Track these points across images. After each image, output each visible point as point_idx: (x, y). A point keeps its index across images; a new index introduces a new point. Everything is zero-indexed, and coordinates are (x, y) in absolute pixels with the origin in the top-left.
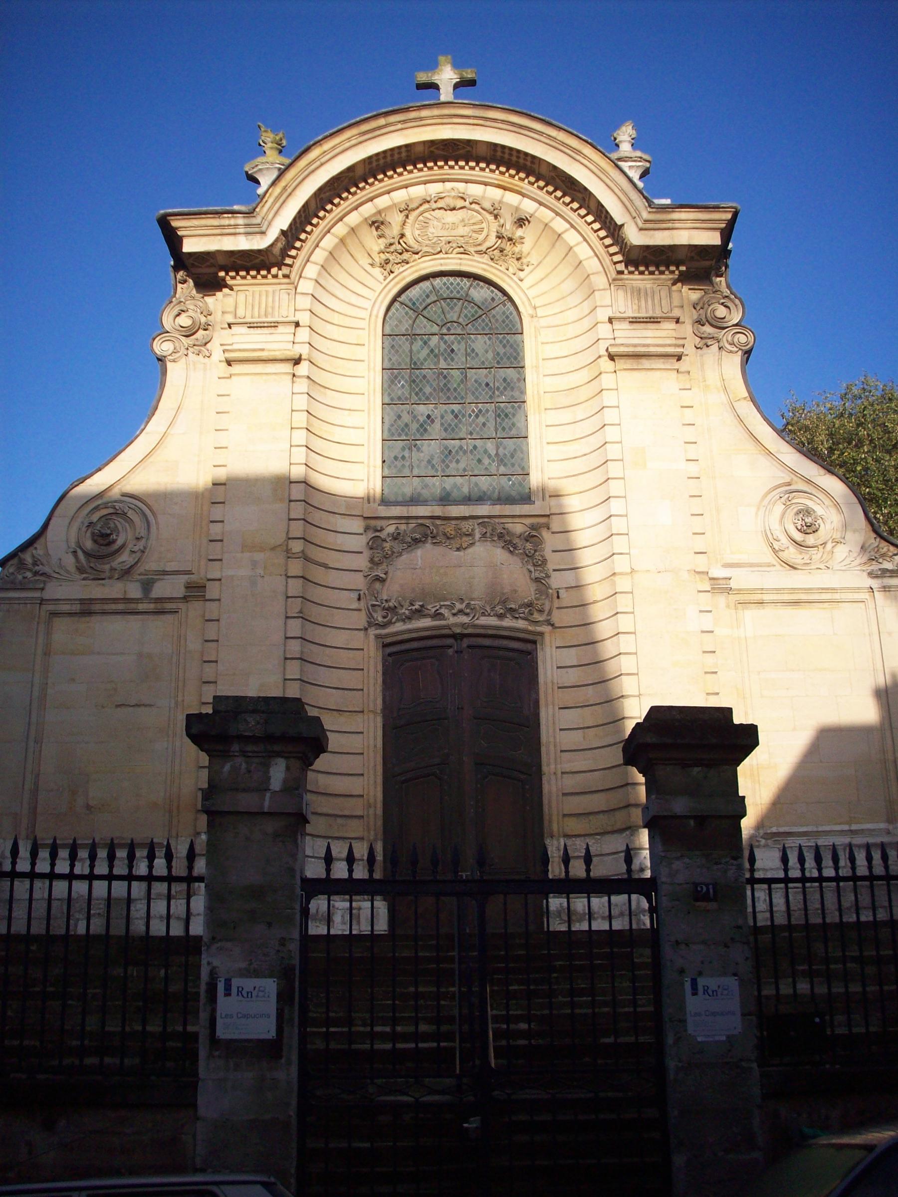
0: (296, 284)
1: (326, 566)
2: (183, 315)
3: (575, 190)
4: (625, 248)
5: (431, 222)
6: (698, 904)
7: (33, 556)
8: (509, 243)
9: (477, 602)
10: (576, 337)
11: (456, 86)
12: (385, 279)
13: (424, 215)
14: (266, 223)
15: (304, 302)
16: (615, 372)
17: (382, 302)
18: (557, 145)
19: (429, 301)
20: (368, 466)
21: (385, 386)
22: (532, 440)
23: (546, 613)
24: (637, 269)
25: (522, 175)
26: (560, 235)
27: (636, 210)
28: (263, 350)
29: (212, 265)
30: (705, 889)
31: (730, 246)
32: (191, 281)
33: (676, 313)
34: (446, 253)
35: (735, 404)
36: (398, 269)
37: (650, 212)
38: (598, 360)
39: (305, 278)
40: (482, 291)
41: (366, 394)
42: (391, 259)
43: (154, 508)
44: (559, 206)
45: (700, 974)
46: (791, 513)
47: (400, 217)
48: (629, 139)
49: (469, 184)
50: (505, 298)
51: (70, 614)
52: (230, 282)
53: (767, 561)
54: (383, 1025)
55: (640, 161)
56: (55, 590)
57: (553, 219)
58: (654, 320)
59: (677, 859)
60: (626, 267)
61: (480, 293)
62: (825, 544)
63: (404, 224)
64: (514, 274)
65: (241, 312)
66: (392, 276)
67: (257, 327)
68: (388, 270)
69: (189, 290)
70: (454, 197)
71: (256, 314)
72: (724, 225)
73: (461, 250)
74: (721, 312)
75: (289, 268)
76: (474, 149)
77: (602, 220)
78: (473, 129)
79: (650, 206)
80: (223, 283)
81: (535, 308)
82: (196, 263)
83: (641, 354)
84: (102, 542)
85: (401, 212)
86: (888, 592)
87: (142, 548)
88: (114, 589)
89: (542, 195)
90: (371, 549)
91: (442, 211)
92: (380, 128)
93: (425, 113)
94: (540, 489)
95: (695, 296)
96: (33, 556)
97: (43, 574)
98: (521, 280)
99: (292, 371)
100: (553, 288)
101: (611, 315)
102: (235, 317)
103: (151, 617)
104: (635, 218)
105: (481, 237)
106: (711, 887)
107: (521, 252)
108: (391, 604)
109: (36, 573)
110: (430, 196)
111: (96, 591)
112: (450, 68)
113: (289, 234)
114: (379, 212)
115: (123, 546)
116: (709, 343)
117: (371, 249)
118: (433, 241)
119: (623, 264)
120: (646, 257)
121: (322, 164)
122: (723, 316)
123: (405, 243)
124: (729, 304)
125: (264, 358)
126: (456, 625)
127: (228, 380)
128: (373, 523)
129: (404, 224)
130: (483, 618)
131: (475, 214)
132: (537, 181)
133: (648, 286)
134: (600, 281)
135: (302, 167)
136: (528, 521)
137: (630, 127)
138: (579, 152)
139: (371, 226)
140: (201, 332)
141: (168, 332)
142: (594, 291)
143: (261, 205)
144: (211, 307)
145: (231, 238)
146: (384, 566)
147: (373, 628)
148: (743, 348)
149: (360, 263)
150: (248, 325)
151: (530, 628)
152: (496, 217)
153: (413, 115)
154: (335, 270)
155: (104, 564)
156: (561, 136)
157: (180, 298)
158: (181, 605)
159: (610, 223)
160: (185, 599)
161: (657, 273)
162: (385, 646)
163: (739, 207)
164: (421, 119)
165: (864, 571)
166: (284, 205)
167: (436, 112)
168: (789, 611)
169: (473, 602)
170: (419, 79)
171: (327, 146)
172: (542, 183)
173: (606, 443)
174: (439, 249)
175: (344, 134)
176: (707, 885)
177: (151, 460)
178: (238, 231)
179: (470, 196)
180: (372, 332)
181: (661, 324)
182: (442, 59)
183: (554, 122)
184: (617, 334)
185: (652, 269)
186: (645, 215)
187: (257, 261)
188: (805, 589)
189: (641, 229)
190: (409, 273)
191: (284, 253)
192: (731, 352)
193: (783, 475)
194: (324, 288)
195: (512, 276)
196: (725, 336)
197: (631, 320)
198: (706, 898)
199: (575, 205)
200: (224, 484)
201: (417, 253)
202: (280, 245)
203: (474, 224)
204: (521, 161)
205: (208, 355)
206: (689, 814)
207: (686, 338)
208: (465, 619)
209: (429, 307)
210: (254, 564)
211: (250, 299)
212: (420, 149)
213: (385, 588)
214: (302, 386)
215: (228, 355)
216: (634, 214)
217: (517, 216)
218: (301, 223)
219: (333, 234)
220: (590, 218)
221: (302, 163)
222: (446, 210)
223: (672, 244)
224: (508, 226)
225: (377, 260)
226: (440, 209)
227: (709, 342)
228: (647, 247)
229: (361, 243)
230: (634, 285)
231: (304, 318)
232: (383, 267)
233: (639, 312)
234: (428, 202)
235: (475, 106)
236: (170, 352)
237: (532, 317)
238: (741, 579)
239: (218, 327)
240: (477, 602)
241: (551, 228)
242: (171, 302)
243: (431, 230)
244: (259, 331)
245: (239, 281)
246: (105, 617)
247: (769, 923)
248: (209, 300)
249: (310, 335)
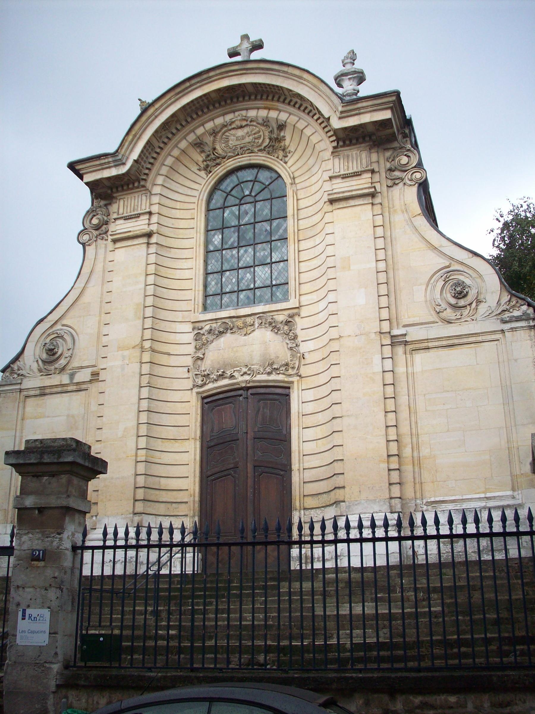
1: (169, 354)
2: (94, 218)
5: (229, 138)
6: (32, 563)
7: (18, 366)
9: (255, 366)
12: (207, 176)
13: (226, 134)
17: (205, 191)
23: (296, 369)
28: (130, 231)
30: (37, 553)
41: (195, 248)
43: (77, 331)
45: (28, 606)
46: (448, 287)
47: (212, 138)
51: (35, 396)
53: (432, 320)
54: (95, 630)
56: (27, 384)
59: (25, 534)
62: (470, 304)
66: (211, 174)
70: (240, 120)
73: (249, 151)
74: (404, 160)
84: (50, 353)
86: (515, 332)
87: (70, 355)
88: (55, 380)
90: (196, 340)
91: (235, 130)
92: (187, 88)
96: (18, 366)
97: (22, 375)
102: (118, 214)
103: (74, 393)
105: (260, 141)
106: (41, 552)
108: (206, 373)
109: (19, 375)
111: (48, 381)
115: (61, 355)
124: (410, 154)
126: (242, 382)
128: (197, 325)
130: (258, 376)
136: (287, 313)
145: (108, 170)
146: (203, 350)
147: (196, 388)
151: (286, 379)
155: (52, 366)
158: (89, 385)
160: (91, 381)
162: (203, 398)
164: (210, 77)
165: (498, 319)
168: (446, 351)
169: (253, 367)
176: (39, 551)
178: (110, 165)
179: (249, 117)
186: (340, 109)
188: (457, 336)
190: (220, 171)
192: (410, 185)
193: (443, 261)
196: (407, 176)
198: (38, 559)
201: (224, 158)
203: (255, 134)
206: (33, 507)
208: (247, 378)
210: (124, 357)
213: (204, 363)
225: (202, 166)
226: (233, 129)
227: (397, 182)
231: (155, 209)
234: (226, 126)
236: (87, 240)
238: (414, 334)
240: (255, 366)
243: (230, 142)
244: (130, 221)
246: (52, 396)
247: (425, 562)
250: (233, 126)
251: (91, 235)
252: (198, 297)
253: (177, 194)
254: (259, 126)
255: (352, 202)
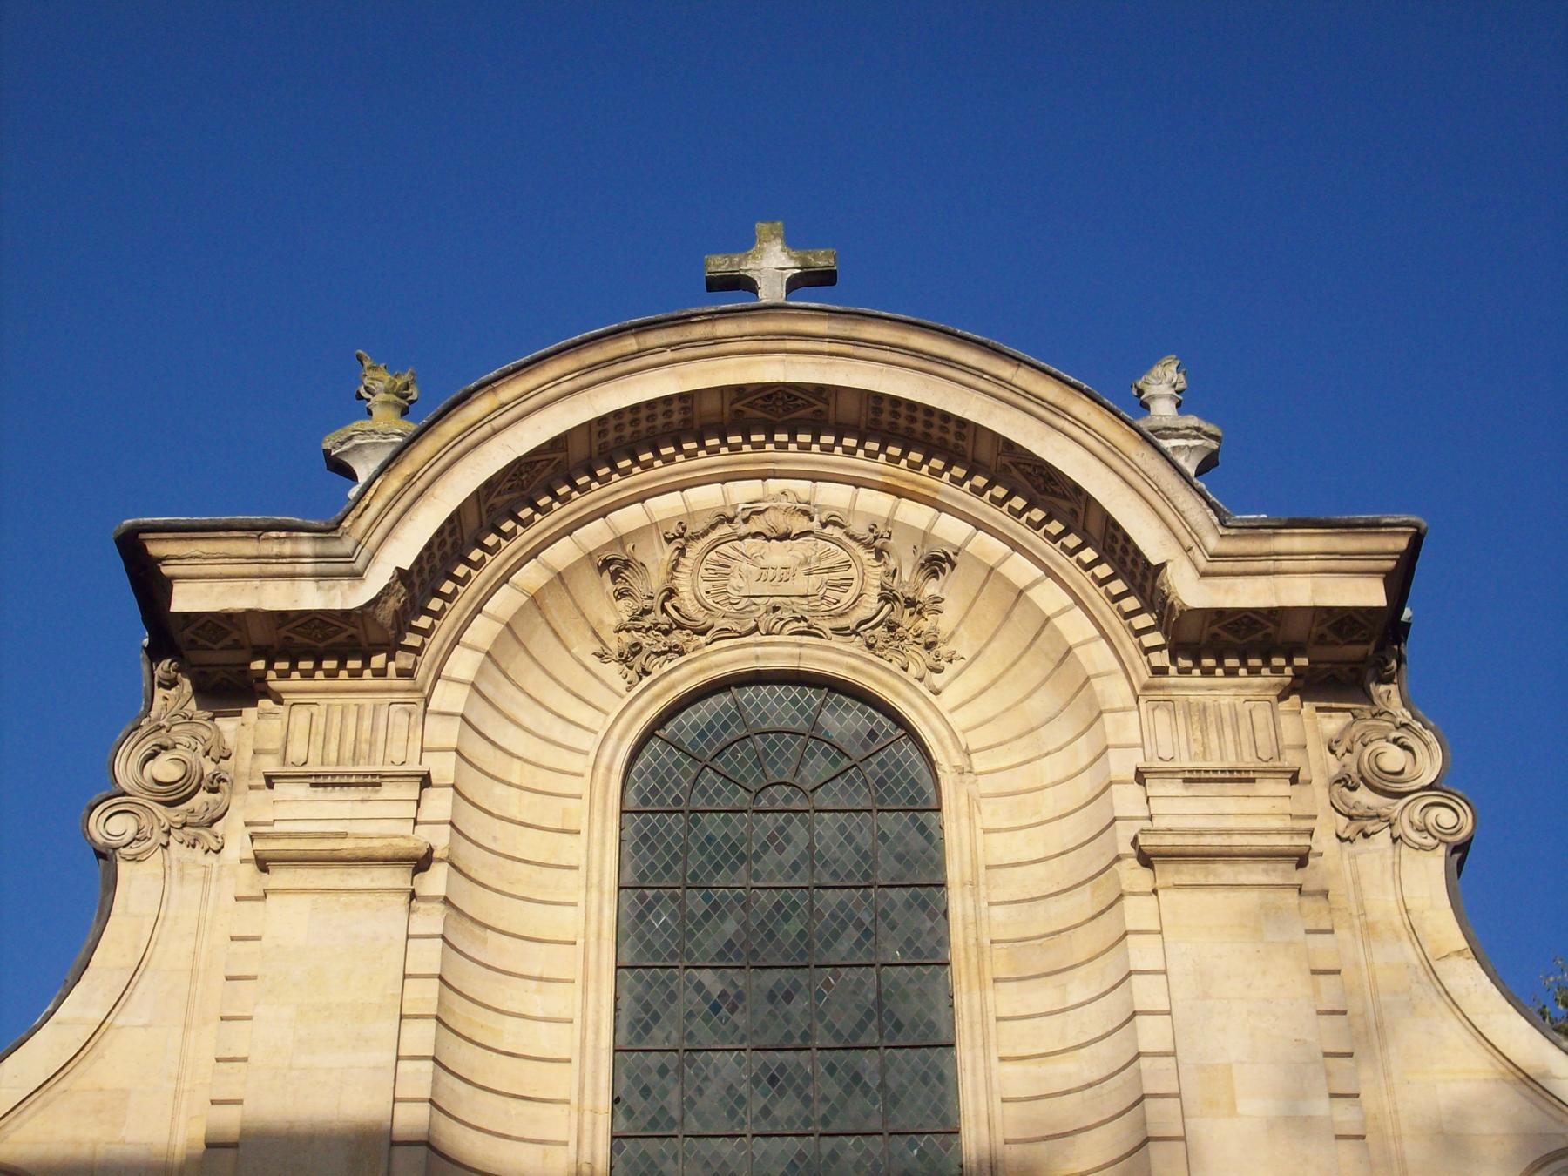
0: (427, 692)
2: (164, 757)
3: (1054, 493)
4: (1169, 617)
5: (734, 565)
8: (908, 611)
10: (1061, 817)
11: (793, 285)
13: (718, 549)
14: (365, 554)
15: (444, 733)
16: (1155, 892)
17: (621, 738)
18: (1013, 397)
19: (727, 737)
20: (580, 1110)
21: (624, 925)
22: (966, 1053)
24: (1197, 663)
25: (937, 463)
26: (1021, 592)
27: (1193, 531)
29: (237, 646)
31: (1407, 613)
32: (187, 681)
33: (1291, 759)
34: (768, 633)
35: (1438, 966)
36: (659, 667)
37: (1221, 536)
38: (1115, 866)
39: (449, 679)
40: (849, 718)
41: (580, 941)
42: (644, 642)
44: (1018, 529)
47: (669, 552)
48: (1172, 391)
49: (819, 484)
50: (901, 732)
52: (276, 684)
55: (1196, 437)
57: (1006, 557)
58: (1240, 777)
60: (1173, 660)
61: (844, 722)
63: (674, 569)
64: (921, 680)
65: (297, 751)
66: (646, 680)
67: (334, 785)
68: (637, 667)
69: (181, 703)
71: (333, 756)
72: (1390, 565)
75: (412, 656)
76: (832, 408)
77: (1116, 557)
78: (830, 364)
79: (1222, 523)
80: (259, 686)
81: (968, 753)
82: (201, 642)
83: (1214, 850)
85: (669, 541)
89: (981, 507)
91: (760, 541)
92: (624, 358)
93: (724, 328)
94: (986, 1166)
95: (1333, 724)
98: (937, 693)
99: (409, 886)
100: (1008, 709)
101: (1142, 764)
102: (284, 761)
104: (1190, 549)
105: (846, 598)
107: (935, 631)
110: (735, 506)
112: (780, 247)
113: (417, 581)
114: (620, 541)
116: (1369, 829)
117: (601, 622)
118: (737, 607)
119: (1166, 652)
120: (1215, 636)
121: (495, 432)
122: (1398, 769)
123: (677, 609)
124: (1411, 741)
125: (344, 854)
127: (260, 904)
129: (674, 569)
131: (833, 547)
132: (969, 476)
133: (1225, 701)
134: (1115, 691)
135: (451, 435)
137: (1174, 367)
138: (1061, 411)
139: (601, 569)
140: (202, 796)
141: (125, 794)
142: (1101, 713)
143: (354, 514)
144: (230, 740)
145: (284, 584)
148: (1449, 839)
149: (573, 651)
150: (313, 780)
152: (879, 554)
153: (698, 331)
154: (519, 664)
156: (1024, 378)
157: (158, 719)
159: (1134, 562)
161: (1242, 671)
163: (1424, 524)
164: (716, 340)
166: (407, 516)
167: (748, 326)
170: (713, 269)
171: (507, 392)
172: (980, 481)
173: (1139, 1055)
174: (753, 624)
175: (547, 368)
177: (63, 1085)
178: (299, 568)
179: (822, 508)
180: (598, 805)
181: (1257, 785)
182: (762, 228)
183: (1007, 349)
184: (1156, 805)
185: (1231, 662)
186: (1213, 543)
187: (341, 637)
189: (1204, 574)
190: (684, 676)
191: (403, 622)
192: (1421, 848)
194: (491, 703)
195: (916, 683)
196: (1407, 813)
197: (1187, 775)
199: (1055, 527)
200: (234, 1146)
201: (703, 633)
202: (393, 603)
204: (935, 432)
205: (216, 847)
207: (1315, 817)
209: (727, 753)
211: (320, 722)
212: (712, 405)
214: (431, 920)
215: (258, 845)
216: (1188, 542)
217: (926, 552)
218: (444, 558)
219: (515, 586)
220: (1088, 555)
221: (451, 427)
222: (768, 539)
223: (1275, 604)
224: (906, 574)
225: (614, 645)
226: (755, 535)
228: (1220, 613)
229: (578, 607)
230: (1191, 699)
231: (443, 767)
232: (625, 661)
233: (1205, 760)
234: (730, 520)
235: (833, 314)
236: (127, 838)
237: (962, 773)
239: (242, 785)
241: (1001, 576)
242: (139, 727)
243: (735, 581)
244: (337, 793)
245: (296, 681)
248: (227, 725)
249: (454, 805)
250: (756, 525)
251: (144, 822)
252: (594, 1137)
253: (512, 729)
254: (854, 544)
255: (1225, 872)
